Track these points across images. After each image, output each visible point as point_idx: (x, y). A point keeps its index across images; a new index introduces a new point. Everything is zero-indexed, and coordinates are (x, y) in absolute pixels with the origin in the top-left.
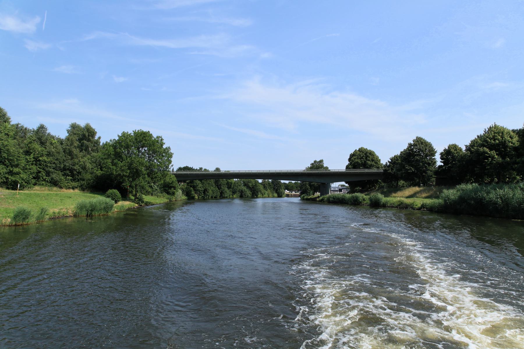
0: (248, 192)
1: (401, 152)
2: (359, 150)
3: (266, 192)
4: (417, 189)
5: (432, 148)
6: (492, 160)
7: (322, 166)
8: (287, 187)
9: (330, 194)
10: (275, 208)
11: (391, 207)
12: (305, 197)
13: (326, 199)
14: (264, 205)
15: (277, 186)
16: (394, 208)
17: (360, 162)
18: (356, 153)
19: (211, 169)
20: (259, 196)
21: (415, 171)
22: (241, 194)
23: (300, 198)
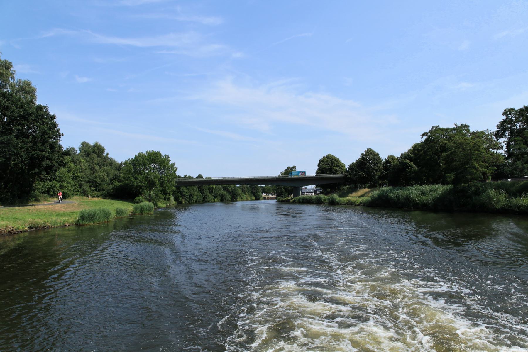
0: (228, 196)
2: (327, 157)
3: (245, 195)
5: (379, 157)
6: (411, 169)
10: (254, 209)
12: (281, 199)
15: (254, 190)
16: (341, 206)
18: (324, 159)
19: (195, 176)
20: (238, 199)
22: (222, 198)
23: (276, 200)
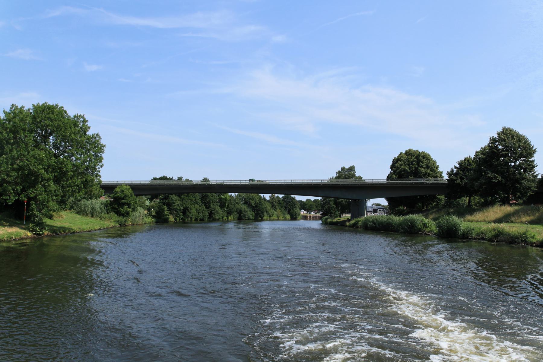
0: (249, 212)
1: (477, 152)
2: (406, 153)
3: (275, 212)
4: (508, 209)
5: (529, 144)
7: (353, 175)
8: (304, 206)
9: (366, 216)
11: (479, 239)
12: (329, 220)
13: (360, 223)
14: (273, 231)
15: (290, 205)
17: (409, 171)
18: (402, 157)
20: (265, 218)
21: (502, 181)
23: (320, 222)
